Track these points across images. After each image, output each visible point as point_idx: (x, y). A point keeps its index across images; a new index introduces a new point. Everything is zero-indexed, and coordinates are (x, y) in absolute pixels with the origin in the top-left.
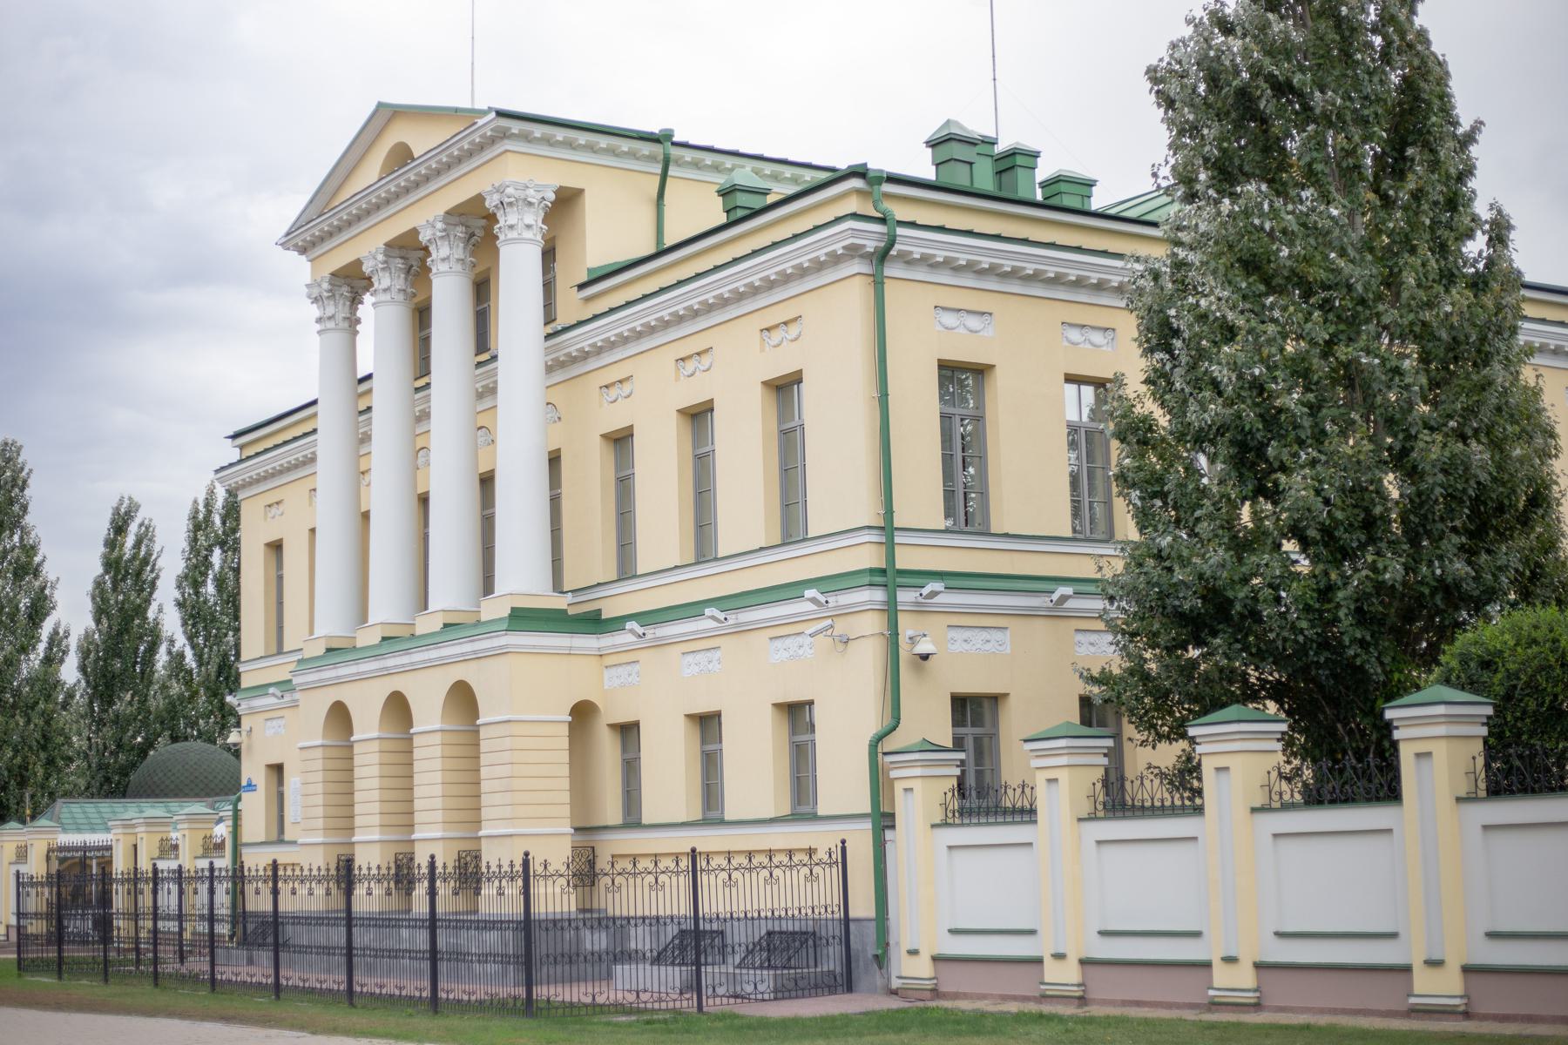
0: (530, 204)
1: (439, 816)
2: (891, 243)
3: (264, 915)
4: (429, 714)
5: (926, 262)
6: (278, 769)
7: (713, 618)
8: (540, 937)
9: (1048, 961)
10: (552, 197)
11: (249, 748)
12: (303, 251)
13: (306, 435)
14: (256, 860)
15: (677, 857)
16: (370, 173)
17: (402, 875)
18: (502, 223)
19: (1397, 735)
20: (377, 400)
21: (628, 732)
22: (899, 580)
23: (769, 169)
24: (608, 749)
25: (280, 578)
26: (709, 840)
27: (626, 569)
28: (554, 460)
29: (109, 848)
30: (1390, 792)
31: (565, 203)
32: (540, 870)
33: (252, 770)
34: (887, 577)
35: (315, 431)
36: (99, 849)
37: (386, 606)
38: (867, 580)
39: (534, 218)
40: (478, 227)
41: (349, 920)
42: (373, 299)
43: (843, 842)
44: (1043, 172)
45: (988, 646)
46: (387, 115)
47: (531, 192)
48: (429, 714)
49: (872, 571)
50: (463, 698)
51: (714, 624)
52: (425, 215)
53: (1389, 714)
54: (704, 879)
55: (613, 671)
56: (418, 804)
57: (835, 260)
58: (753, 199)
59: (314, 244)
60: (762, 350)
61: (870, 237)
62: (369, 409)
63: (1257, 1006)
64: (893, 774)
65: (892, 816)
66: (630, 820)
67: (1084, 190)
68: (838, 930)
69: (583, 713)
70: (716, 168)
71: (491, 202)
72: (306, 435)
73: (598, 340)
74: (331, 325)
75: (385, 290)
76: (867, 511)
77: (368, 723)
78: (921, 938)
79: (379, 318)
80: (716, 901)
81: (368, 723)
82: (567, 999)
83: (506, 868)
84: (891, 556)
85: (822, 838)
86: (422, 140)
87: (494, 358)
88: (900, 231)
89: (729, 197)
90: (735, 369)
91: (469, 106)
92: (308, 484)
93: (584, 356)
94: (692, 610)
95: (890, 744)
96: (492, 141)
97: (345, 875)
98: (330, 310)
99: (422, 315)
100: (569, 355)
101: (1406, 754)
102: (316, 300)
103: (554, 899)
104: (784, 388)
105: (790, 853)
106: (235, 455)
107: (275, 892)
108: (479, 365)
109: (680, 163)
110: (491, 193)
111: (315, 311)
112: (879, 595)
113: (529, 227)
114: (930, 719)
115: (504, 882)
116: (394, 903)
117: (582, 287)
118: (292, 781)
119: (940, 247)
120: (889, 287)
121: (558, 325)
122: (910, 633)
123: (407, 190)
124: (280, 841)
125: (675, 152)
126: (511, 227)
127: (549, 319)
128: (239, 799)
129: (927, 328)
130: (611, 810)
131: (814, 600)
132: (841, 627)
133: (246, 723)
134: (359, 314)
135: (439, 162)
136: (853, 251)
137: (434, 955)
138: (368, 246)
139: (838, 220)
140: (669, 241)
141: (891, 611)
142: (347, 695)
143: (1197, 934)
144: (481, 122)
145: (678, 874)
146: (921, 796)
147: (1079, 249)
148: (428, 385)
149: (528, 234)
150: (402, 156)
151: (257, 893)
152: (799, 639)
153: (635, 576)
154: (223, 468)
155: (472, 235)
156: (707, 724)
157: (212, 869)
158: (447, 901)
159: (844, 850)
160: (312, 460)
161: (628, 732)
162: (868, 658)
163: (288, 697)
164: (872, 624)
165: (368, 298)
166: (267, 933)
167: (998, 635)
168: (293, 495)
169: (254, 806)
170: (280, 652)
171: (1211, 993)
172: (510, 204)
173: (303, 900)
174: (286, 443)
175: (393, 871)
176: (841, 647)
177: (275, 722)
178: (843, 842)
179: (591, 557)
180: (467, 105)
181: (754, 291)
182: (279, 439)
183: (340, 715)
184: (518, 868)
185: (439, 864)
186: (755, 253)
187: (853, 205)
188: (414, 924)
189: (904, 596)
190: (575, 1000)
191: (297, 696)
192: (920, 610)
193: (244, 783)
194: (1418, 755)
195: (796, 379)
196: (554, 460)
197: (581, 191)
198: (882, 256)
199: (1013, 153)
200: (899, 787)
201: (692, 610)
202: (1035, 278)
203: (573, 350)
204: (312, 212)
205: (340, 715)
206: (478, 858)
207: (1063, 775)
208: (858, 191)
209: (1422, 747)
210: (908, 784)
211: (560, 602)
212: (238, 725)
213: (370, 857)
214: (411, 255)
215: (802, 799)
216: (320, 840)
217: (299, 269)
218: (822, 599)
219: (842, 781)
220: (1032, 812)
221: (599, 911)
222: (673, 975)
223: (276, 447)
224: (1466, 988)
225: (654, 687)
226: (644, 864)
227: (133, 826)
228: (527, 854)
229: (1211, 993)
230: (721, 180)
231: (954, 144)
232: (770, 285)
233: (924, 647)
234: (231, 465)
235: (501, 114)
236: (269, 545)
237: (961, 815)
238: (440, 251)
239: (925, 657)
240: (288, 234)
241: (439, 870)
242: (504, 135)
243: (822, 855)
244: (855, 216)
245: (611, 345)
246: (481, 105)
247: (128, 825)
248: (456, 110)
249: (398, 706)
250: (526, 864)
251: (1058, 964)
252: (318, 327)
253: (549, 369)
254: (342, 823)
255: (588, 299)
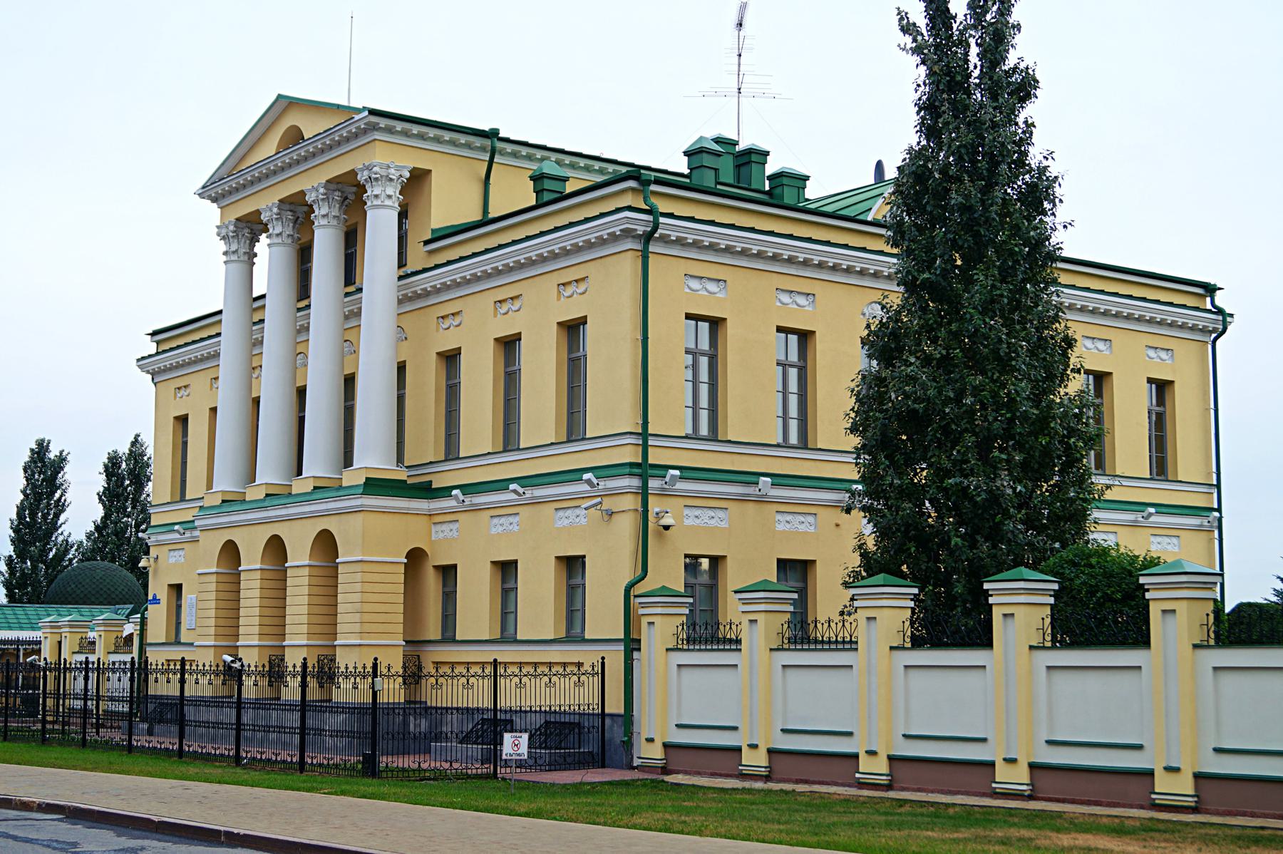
0: (391, 180)
1: (305, 629)
2: (656, 226)
3: (173, 698)
4: (300, 555)
5: (680, 242)
6: (177, 589)
7: (515, 491)
8: (381, 719)
9: (745, 750)
10: (408, 175)
11: (156, 571)
12: (214, 200)
13: (210, 337)
14: (156, 657)
15: (483, 665)
16: (269, 148)
17: (275, 671)
18: (369, 193)
19: (991, 600)
20: (268, 315)
21: (448, 572)
22: (650, 472)
23: (567, 160)
24: (432, 584)
25: (185, 444)
26: (506, 654)
27: (451, 451)
28: (401, 368)
29: (40, 642)
30: (982, 638)
31: (417, 180)
32: (385, 671)
33: (158, 588)
34: (643, 469)
35: (219, 335)
36: (30, 643)
37: (269, 472)
38: (627, 470)
39: (393, 190)
40: (351, 195)
41: (240, 705)
42: (268, 241)
43: (603, 658)
44: (770, 169)
45: (713, 522)
46: (285, 104)
47: (392, 171)
48: (300, 555)
49: (631, 465)
50: (326, 543)
51: (516, 497)
52: (312, 182)
53: (986, 586)
54: (501, 682)
55: (439, 527)
56: (288, 620)
57: (614, 238)
58: (560, 182)
59: (223, 196)
60: (559, 299)
61: (641, 223)
62: (262, 321)
63: (889, 787)
64: (641, 611)
65: (639, 641)
66: (449, 634)
67: (799, 183)
68: (598, 722)
69: (415, 557)
70: (529, 158)
71: (362, 177)
72: (210, 337)
73: (438, 283)
74: (234, 257)
75: (278, 235)
76: (630, 422)
77: (252, 559)
78: (654, 732)
79: (269, 257)
80: (510, 698)
81: (252, 559)
82: (400, 765)
83: (360, 669)
84: (645, 455)
85: (588, 656)
86: (311, 127)
87: (360, 290)
88: (662, 220)
89: (538, 182)
90: (537, 315)
91: (346, 104)
92: (212, 374)
93: (426, 294)
94: (500, 485)
95: (640, 589)
96: (365, 131)
97: (275, 671)
98: (234, 247)
99: (304, 254)
100: (415, 292)
101: (1155, 611)
102: (223, 238)
103: (392, 692)
104: (573, 329)
105: (565, 665)
106: (152, 349)
107: (182, 681)
108: (347, 294)
109: (503, 153)
110: (362, 170)
111: (222, 246)
112: (636, 482)
113: (390, 197)
114: (668, 572)
115: (358, 679)
116: (268, 693)
117: (427, 243)
118: (188, 597)
119: (691, 231)
120: (652, 258)
121: (409, 269)
122: (657, 510)
123: (298, 162)
124: (177, 642)
125: (499, 145)
126: (376, 196)
127: (402, 264)
128: (146, 609)
129: (680, 287)
130: (433, 630)
131: (589, 482)
132: (608, 504)
133: (153, 552)
134: (256, 250)
135: (324, 144)
136: (627, 233)
137: (239, 725)
138: (266, 202)
139: (618, 210)
140: (493, 214)
141: (644, 493)
142: (237, 536)
143: (1139, 747)
144: (357, 117)
145: (483, 677)
146: (661, 630)
147: (791, 237)
148: (308, 307)
149: (388, 202)
150: (295, 136)
151: (156, 681)
152: (578, 511)
153: (458, 458)
154: (143, 358)
155: (346, 198)
156: (507, 569)
157: (87, 662)
158: (314, 693)
159: (603, 664)
160: (217, 355)
161: (448, 572)
162: (626, 526)
163: (188, 534)
164: (631, 502)
165: (263, 237)
166: (174, 712)
167: (721, 514)
168: (199, 382)
169: (157, 615)
170: (183, 499)
171: (857, 775)
172: (376, 179)
173: (199, 687)
174: (194, 342)
175: (267, 669)
176: (606, 518)
177: (176, 553)
178: (603, 658)
179: (425, 445)
180: (343, 102)
181: (554, 256)
182: (189, 339)
183: (231, 551)
184: (369, 669)
185: (310, 665)
186: (557, 229)
187: (627, 200)
188: (290, 707)
189: (653, 484)
190: (406, 766)
191: (196, 533)
192: (663, 494)
193: (150, 597)
194: (1005, 615)
195: (458, 352)
196: (401, 368)
197: (430, 171)
198: (648, 237)
199: (750, 152)
200: (644, 621)
201: (500, 485)
202: (760, 255)
203: (418, 289)
204: (223, 172)
205: (231, 551)
206: (333, 660)
207: (761, 618)
208: (633, 189)
209: (1008, 610)
210: (651, 619)
211: (402, 475)
212: (147, 553)
213: (251, 658)
214: (299, 212)
215: (573, 633)
216: (212, 643)
217: (212, 213)
218: (595, 481)
219: (603, 617)
220: (738, 641)
221: (421, 702)
222: (475, 749)
223: (187, 344)
224: (1032, 778)
225: (470, 542)
226: (460, 669)
227: (59, 627)
228: (376, 659)
229: (857, 775)
230: (534, 166)
231: (705, 155)
232: (566, 253)
233: (667, 520)
234: (150, 356)
235: (373, 112)
236: (176, 418)
237: (688, 643)
238: (321, 210)
239: (667, 528)
240: (204, 187)
241: (310, 669)
242: (375, 128)
243: (587, 667)
244: (630, 208)
245: (446, 288)
246: (357, 104)
247: (54, 626)
248: (338, 106)
249: (276, 547)
250: (375, 666)
251: (753, 752)
252: (224, 258)
253: (400, 302)
254: (326, 629)
255: (431, 252)
